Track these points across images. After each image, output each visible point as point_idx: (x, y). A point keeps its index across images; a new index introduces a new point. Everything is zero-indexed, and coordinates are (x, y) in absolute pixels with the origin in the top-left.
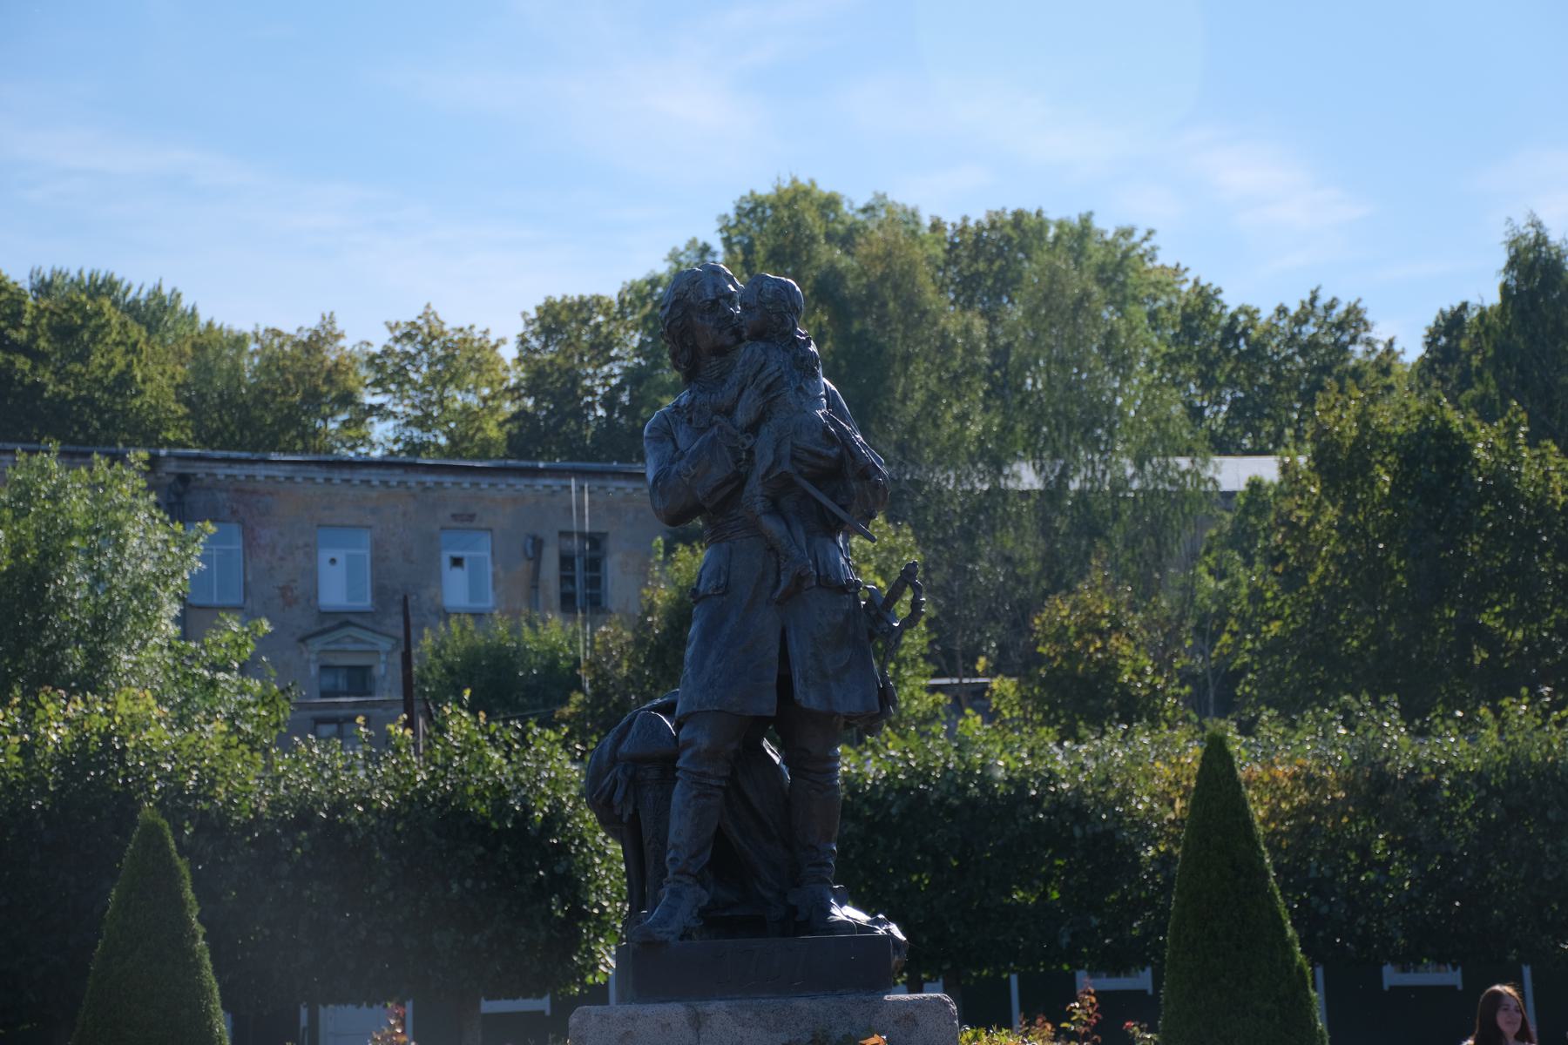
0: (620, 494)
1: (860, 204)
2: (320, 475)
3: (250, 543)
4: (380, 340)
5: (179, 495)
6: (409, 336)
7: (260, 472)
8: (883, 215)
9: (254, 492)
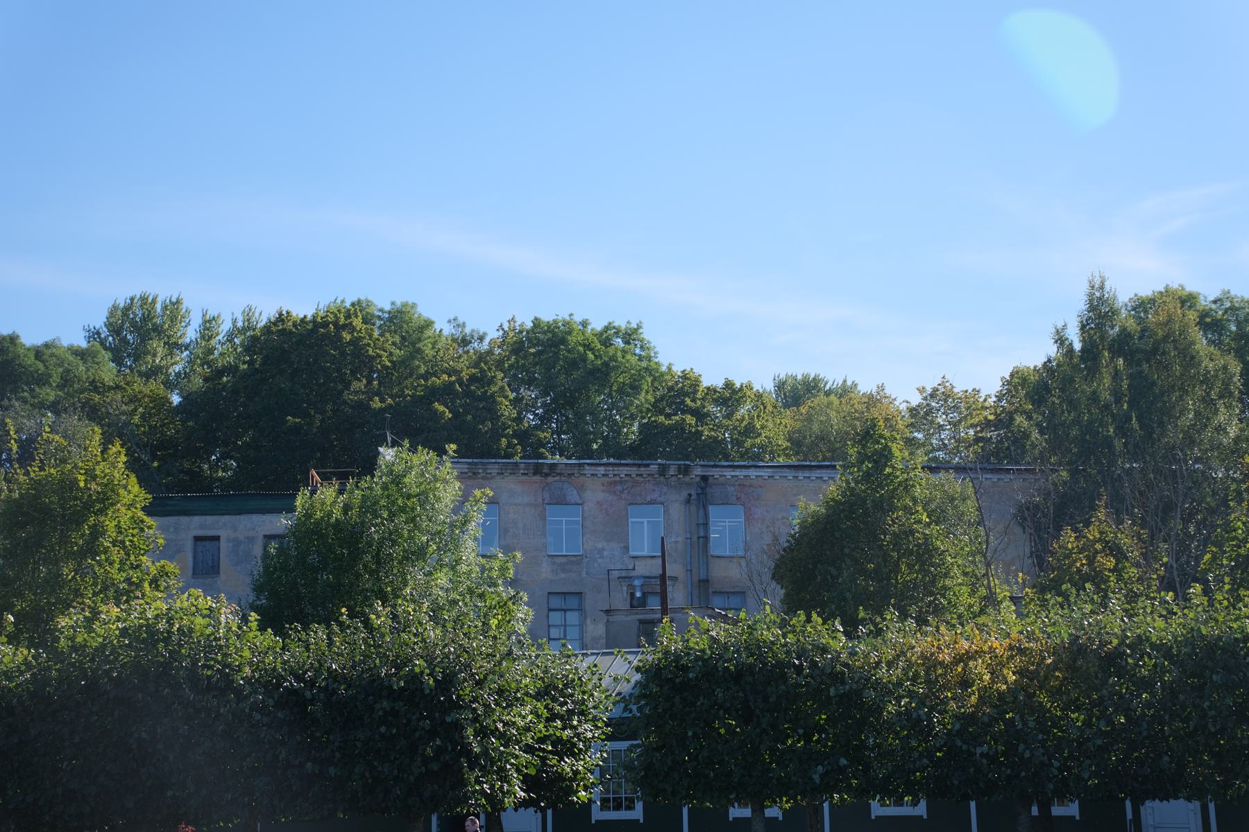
1: (1212, 298)
2: (790, 474)
3: (749, 518)
4: (916, 400)
5: (703, 489)
6: (933, 395)
7: (753, 473)
8: (1228, 305)
9: (751, 486)
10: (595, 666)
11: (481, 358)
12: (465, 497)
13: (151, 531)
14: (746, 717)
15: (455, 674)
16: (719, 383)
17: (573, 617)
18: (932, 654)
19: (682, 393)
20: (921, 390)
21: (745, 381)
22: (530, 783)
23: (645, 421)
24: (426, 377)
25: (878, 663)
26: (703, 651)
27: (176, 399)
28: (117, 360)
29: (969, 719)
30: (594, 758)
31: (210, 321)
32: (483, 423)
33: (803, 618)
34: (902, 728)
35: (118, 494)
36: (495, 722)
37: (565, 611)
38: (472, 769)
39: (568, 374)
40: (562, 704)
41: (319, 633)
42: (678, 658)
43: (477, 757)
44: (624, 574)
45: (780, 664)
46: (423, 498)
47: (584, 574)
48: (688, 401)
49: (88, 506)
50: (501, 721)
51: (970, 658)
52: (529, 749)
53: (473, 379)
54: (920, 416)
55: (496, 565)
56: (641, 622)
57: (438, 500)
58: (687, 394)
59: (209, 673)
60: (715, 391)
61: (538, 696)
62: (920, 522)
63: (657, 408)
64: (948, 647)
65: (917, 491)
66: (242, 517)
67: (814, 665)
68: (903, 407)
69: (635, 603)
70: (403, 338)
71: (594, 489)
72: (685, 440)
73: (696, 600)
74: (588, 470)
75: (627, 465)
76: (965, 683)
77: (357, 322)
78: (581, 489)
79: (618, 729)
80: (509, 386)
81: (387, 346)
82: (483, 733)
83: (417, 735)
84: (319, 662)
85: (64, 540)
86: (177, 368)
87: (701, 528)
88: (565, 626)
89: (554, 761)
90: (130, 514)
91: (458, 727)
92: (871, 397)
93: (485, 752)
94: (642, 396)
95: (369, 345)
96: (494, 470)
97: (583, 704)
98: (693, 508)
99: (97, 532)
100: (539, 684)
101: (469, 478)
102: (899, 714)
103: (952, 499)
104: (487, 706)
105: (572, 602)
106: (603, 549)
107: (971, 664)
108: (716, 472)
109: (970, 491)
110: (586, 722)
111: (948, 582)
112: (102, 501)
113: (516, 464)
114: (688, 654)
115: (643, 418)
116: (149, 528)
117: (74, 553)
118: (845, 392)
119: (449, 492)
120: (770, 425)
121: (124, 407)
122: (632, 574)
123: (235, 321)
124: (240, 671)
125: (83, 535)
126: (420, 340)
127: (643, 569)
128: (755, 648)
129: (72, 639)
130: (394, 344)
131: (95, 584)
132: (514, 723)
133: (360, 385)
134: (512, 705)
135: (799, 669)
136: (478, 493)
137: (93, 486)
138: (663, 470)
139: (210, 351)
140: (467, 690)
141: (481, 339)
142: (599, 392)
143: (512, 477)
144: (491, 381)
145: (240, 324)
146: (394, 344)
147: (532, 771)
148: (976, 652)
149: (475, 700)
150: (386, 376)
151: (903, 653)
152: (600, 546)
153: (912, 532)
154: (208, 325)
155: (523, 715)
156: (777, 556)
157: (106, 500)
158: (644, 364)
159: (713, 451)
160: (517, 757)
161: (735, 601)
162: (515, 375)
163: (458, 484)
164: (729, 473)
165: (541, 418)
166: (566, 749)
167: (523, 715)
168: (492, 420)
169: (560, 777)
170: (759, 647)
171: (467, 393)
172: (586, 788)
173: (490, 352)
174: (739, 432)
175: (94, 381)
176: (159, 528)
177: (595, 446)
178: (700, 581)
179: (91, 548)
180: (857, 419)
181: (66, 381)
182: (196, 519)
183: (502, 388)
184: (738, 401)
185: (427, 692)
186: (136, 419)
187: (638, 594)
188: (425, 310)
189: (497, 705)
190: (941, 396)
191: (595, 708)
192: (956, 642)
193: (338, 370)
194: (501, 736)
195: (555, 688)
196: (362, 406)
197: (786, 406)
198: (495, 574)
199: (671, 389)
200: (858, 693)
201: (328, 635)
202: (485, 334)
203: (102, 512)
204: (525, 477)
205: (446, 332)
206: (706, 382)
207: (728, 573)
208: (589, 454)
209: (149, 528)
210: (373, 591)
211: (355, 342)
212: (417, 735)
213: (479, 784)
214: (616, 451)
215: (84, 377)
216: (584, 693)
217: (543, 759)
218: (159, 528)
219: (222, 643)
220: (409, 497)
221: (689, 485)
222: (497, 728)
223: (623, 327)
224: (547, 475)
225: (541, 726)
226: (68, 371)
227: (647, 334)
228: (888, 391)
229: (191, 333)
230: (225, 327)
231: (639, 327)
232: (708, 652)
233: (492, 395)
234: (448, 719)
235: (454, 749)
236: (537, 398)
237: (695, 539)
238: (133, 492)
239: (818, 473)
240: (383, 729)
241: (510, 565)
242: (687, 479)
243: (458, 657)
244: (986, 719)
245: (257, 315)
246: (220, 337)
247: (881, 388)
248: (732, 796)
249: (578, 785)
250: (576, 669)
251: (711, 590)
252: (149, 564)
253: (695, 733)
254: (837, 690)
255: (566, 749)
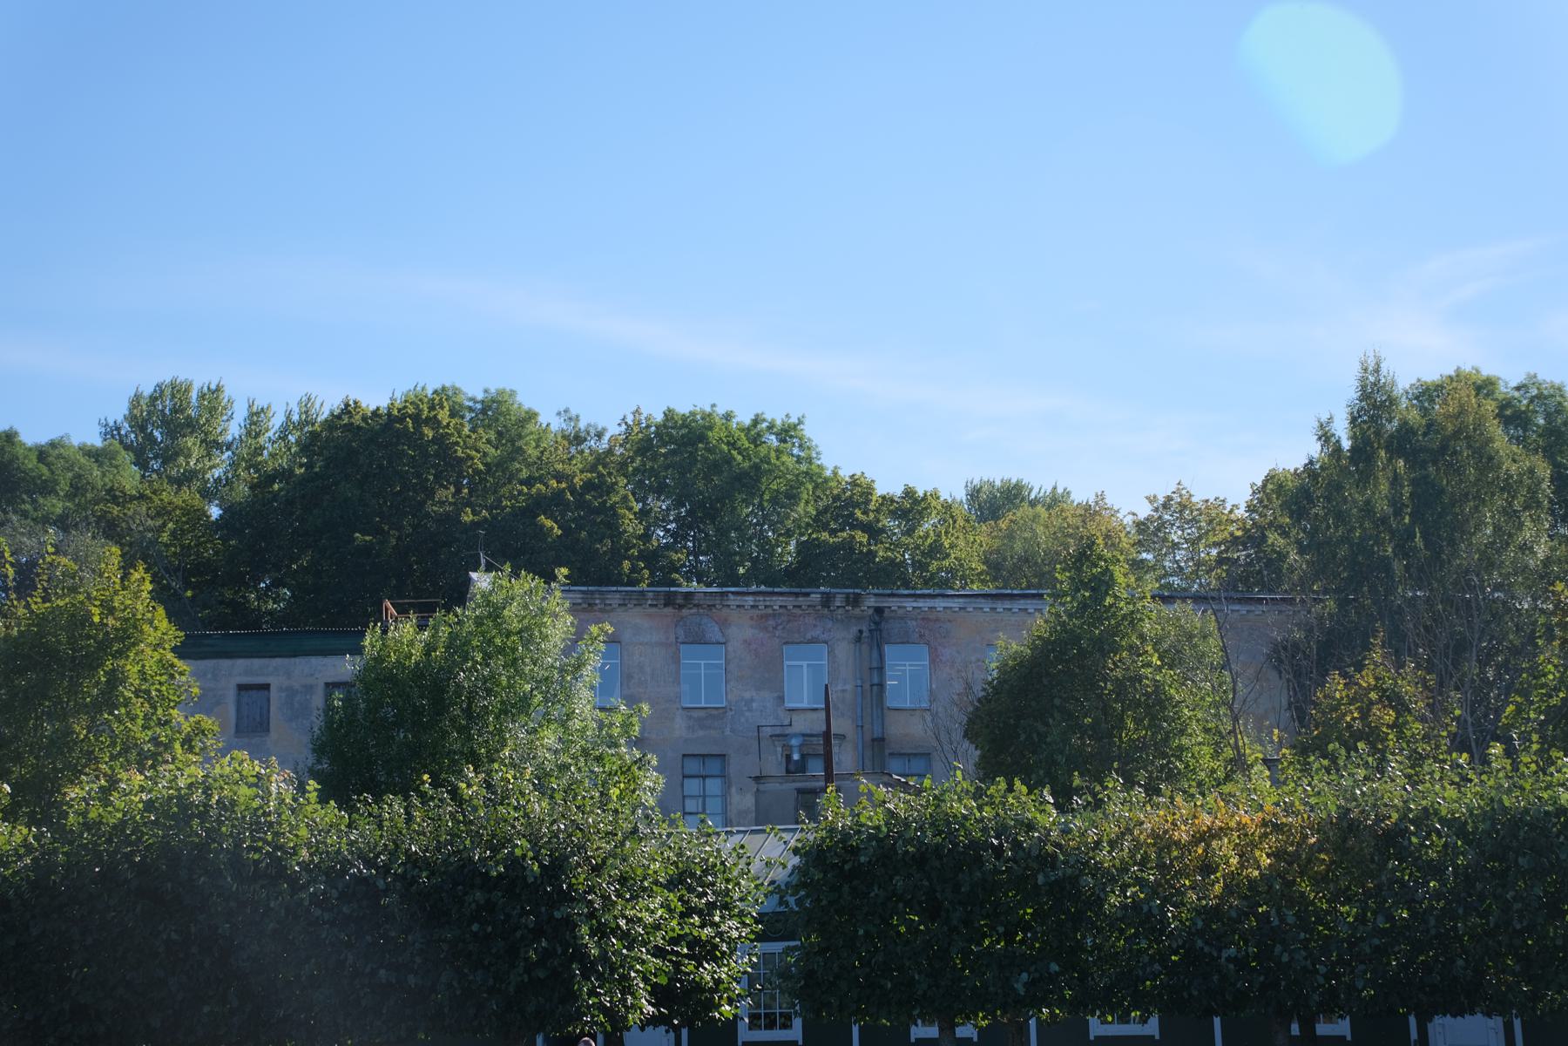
0: (1236, 615)
1: (1514, 384)
2: (986, 605)
3: (934, 660)
4: (1144, 511)
5: (876, 623)
6: (1166, 506)
7: (940, 604)
8: (1534, 392)
9: (937, 620)
10: (742, 847)
11: (601, 459)
12: (580, 633)
13: (184, 678)
14: (933, 912)
15: (567, 858)
16: (897, 491)
17: (714, 786)
18: (1166, 832)
19: (851, 503)
20: (1151, 500)
21: (929, 489)
22: (660, 995)
23: (804, 538)
24: (529, 482)
25: (1098, 844)
26: (878, 828)
27: (215, 512)
28: (142, 463)
29: (1212, 914)
30: (741, 963)
31: (257, 414)
32: (601, 541)
33: (1003, 786)
34: (1129, 926)
35: (142, 632)
36: (616, 918)
37: (704, 777)
38: (586, 977)
39: (707, 479)
40: (700, 896)
41: (394, 806)
42: (846, 836)
43: (594, 964)
44: (778, 731)
45: (974, 845)
46: (526, 635)
47: (728, 732)
48: (858, 513)
49: (104, 646)
50: (624, 917)
51: (1213, 837)
52: (658, 952)
53: (589, 486)
54: (1150, 532)
55: (618, 719)
56: (800, 791)
57: (545, 638)
58: (857, 505)
59: (256, 857)
60: (892, 501)
61: (671, 885)
62: (1149, 665)
63: (819, 522)
64: (1185, 822)
65: (1147, 626)
66: (297, 660)
67: (1017, 845)
68: (1128, 520)
69: (792, 767)
70: (500, 434)
71: (740, 626)
72: (855, 563)
73: (868, 763)
74: (733, 601)
75: (781, 594)
76: (1207, 868)
77: (443, 416)
78: (724, 624)
79: (771, 927)
80: (634, 494)
81: (480, 445)
82: (601, 932)
83: (518, 934)
84: (394, 842)
85: (74, 689)
86: (217, 473)
87: (875, 673)
88: (704, 797)
89: (691, 968)
90: (157, 656)
91: (570, 924)
92: (1087, 508)
93: (604, 957)
94: (801, 508)
95: (457, 443)
96: (615, 600)
97: (727, 895)
98: (865, 647)
99: (115, 679)
100: (672, 870)
101: (584, 610)
102: (1124, 907)
103: (1190, 637)
104: (605, 898)
105: (713, 767)
106: (752, 700)
107: (1214, 844)
108: (893, 603)
109: (1213, 626)
110: (731, 917)
111: (1185, 741)
112: (122, 640)
113: (642, 593)
114: (859, 832)
115: (802, 535)
116: (181, 674)
117: (86, 706)
118: (1055, 501)
119: (559, 628)
120: (961, 543)
121: (150, 522)
122: (789, 731)
123: (288, 418)
124: (295, 853)
125: (98, 683)
126: (520, 437)
127: (801, 724)
128: (943, 824)
129: (84, 814)
130: (489, 441)
131: (113, 744)
132: (640, 920)
133: (445, 494)
134: (637, 897)
135: (998, 851)
136: (594, 629)
137: (111, 621)
138: (827, 600)
139: (259, 450)
140: (581, 877)
141: (599, 435)
142: (747, 503)
143: (638, 609)
144: (611, 489)
145: (295, 418)
146: (489, 441)
147: (663, 980)
148: (1221, 829)
149: (591, 890)
150: (479, 483)
151: (1129, 831)
152: (747, 695)
153: (1139, 679)
154: (256, 419)
155: (651, 909)
156: (971, 709)
157: (126, 637)
158: (803, 467)
159: (889, 576)
160: (643, 962)
161: (918, 765)
162: (641, 482)
163: (570, 619)
164: (910, 604)
165: (674, 535)
166: (705, 951)
167: (651, 909)
168: (611, 537)
169: (698, 987)
170: (949, 824)
171: (581, 504)
172: (730, 1001)
173: (610, 452)
174: (923, 553)
175: (112, 489)
176: (193, 674)
177: (741, 571)
178: (873, 740)
179: (109, 698)
180: (1070, 536)
181: (77, 489)
182: (241, 663)
183: (625, 498)
184: (920, 513)
185: (531, 880)
186: (165, 537)
187: (796, 757)
188: (526, 400)
189: (618, 896)
190: (1177, 507)
191: (741, 900)
192: (1195, 817)
193: (418, 476)
194: (624, 936)
195: (692, 875)
196: (451, 519)
197: (982, 519)
198: (616, 732)
199: (836, 498)
200: (1074, 880)
201: (406, 809)
202: (604, 429)
203: (121, 654)
204: (654, 610)
205: (554, 427)
206: (881, 489)
207: (909, 729)
208: (734, 580)
209: (181, 674)
210: (462, 753)
211: (440, 440)
212: (518, 934)
213: (596, 996)
214: (768, 575)
215: (100, 484)
216: (728, 881)
217: (677, 965)
218: (193, 674)
219: (273, 818)
220: (509, 634)
221: (859, 618)
222: (618, 927)
223: (779, 423)
224: (681, 607)
225: (674, 923)
226: (79, 476)
227: (808, 431)
228: (1109, 501)
229: (234, 429)
230: (277, 422)
231: (800, 422)
232: (884, 829)
233: (613, 507)
234: (557, 915)
235: (565, 951)
236: (668, 509)
237: (867, 686)
238: (161, 629)
239: (1022, 603)
240: (475, 927)
241: (635, 720)
242: (857, 611)
243: (570, 836)
244: (1234, 914)
245: (317, 406)
246: (270, 434)
247: (1101, 497)
248: (916, 1012)
249: (721, 998)
250: (718, 851)
251: (887, 752)
252: (181, 719)
253: (866, 932)
254: (1046, 876)
255: (705, 951)
